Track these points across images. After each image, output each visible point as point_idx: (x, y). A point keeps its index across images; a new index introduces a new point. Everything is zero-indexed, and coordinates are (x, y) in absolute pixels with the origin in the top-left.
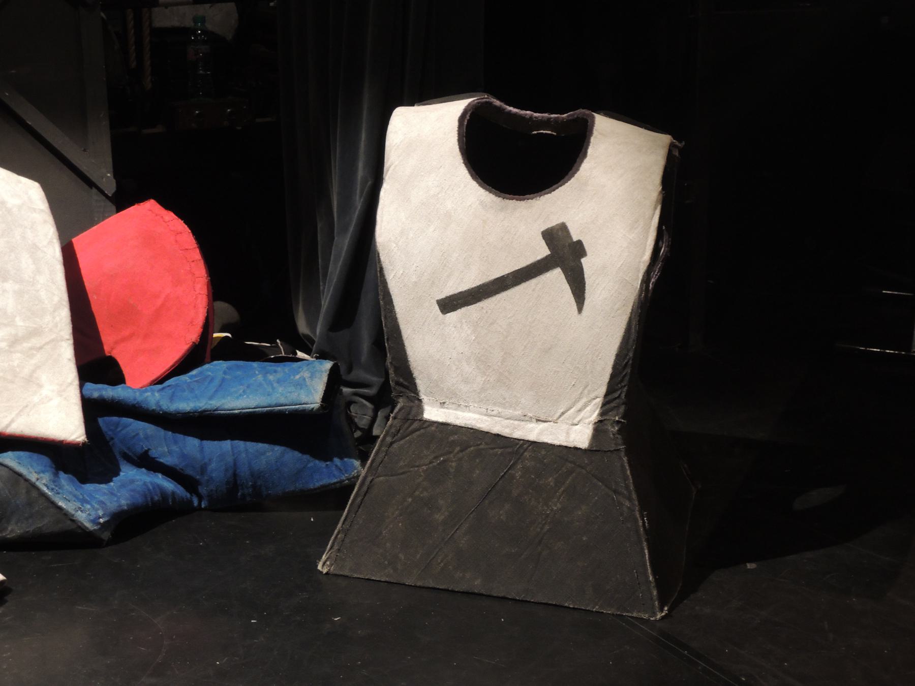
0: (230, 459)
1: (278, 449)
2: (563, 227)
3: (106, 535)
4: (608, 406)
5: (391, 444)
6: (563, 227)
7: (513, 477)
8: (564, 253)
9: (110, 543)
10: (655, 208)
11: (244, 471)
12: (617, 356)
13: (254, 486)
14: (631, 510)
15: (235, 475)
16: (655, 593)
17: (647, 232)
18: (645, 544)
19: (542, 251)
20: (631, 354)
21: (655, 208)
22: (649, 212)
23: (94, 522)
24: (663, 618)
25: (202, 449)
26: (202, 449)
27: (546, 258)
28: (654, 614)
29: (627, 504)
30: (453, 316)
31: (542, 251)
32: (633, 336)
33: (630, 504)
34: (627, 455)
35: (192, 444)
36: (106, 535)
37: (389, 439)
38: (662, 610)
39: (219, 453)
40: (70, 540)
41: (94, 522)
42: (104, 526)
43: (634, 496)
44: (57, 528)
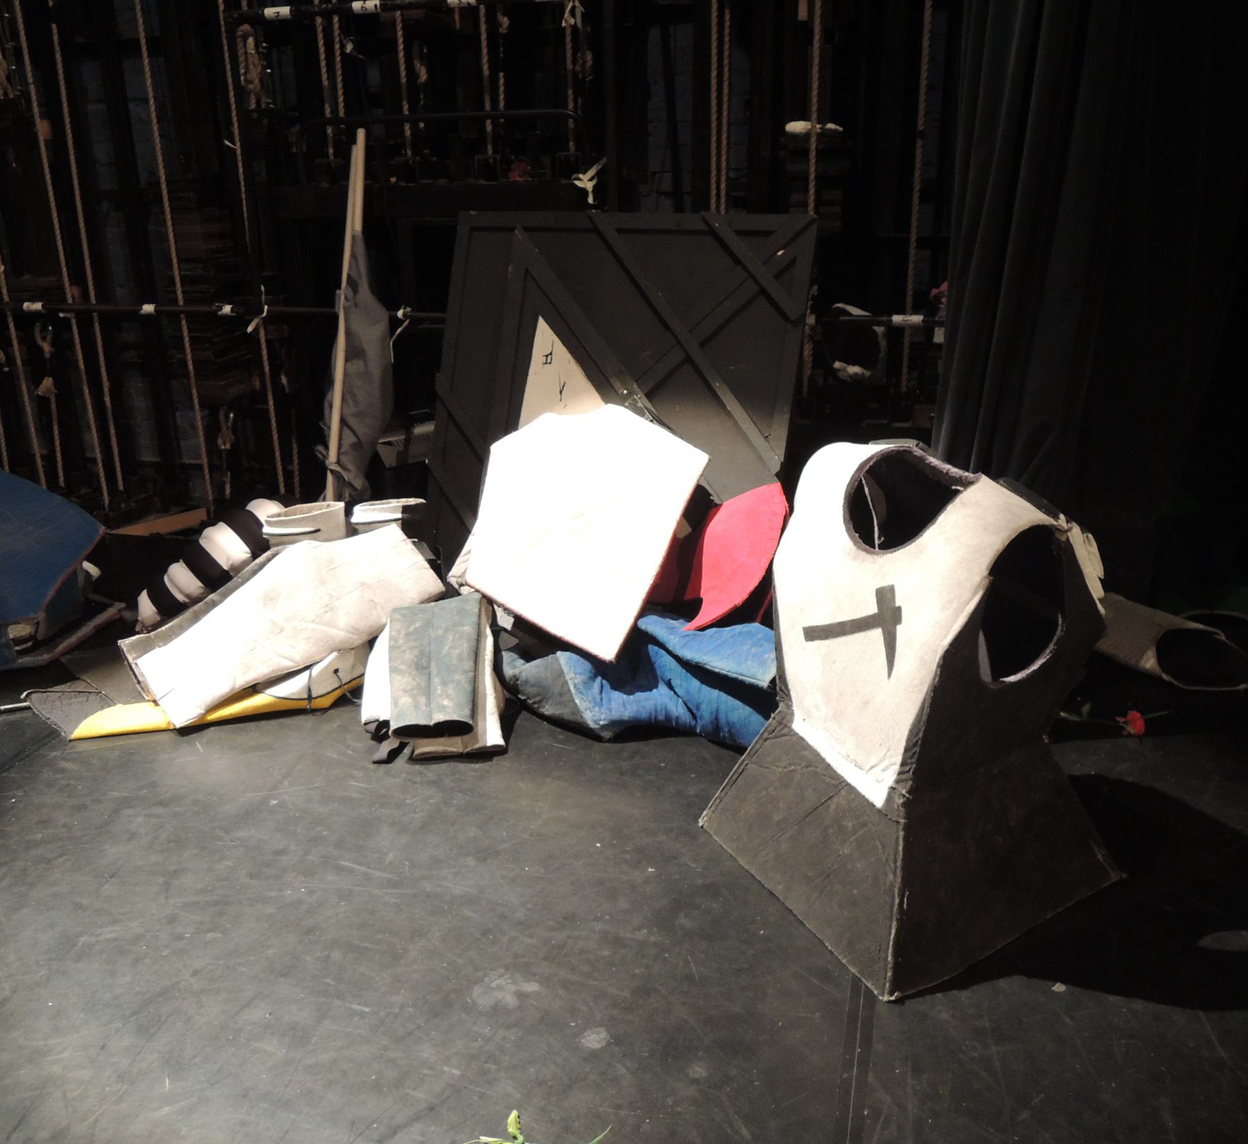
0: (715, 706)
1: (748, 710)
2: (891, 589)
3: (607, 734)
4: (903, 777)
5: (766, 740)
6: (891, 589)
7: (828, 807)
8: (887, 616)
9: (609, 741)
10: (975, 593)
11: (723, 721)
12: (911, 731)
13: (729, 732)
14: (892, 886)
15: (717, 719)
16: (889, 974)
17: (957, 614)
18: (894, 924)
19: (871, 608)
20: (921, 735)
21: (975, 593)
22: (966, 595)
23: (596, 722)
24: (890, 1002)
25: (699, 691)
26: (699, 691)
27: (874, 616)
28: (883, 994)
29: (891, 877)
30: (817, 643)
31: (871, 608)
32: (925, 718)
33: (894, 879)
34: (904, 829)
35: (695, 683)
36: (607, 734)
37: (766, 735)
38: (891, 994)
39: (712, 698)
40: (576, 728)
41: (596, 722)
42: (603, 727)
43: (899, 872)
44: (571, 718)
